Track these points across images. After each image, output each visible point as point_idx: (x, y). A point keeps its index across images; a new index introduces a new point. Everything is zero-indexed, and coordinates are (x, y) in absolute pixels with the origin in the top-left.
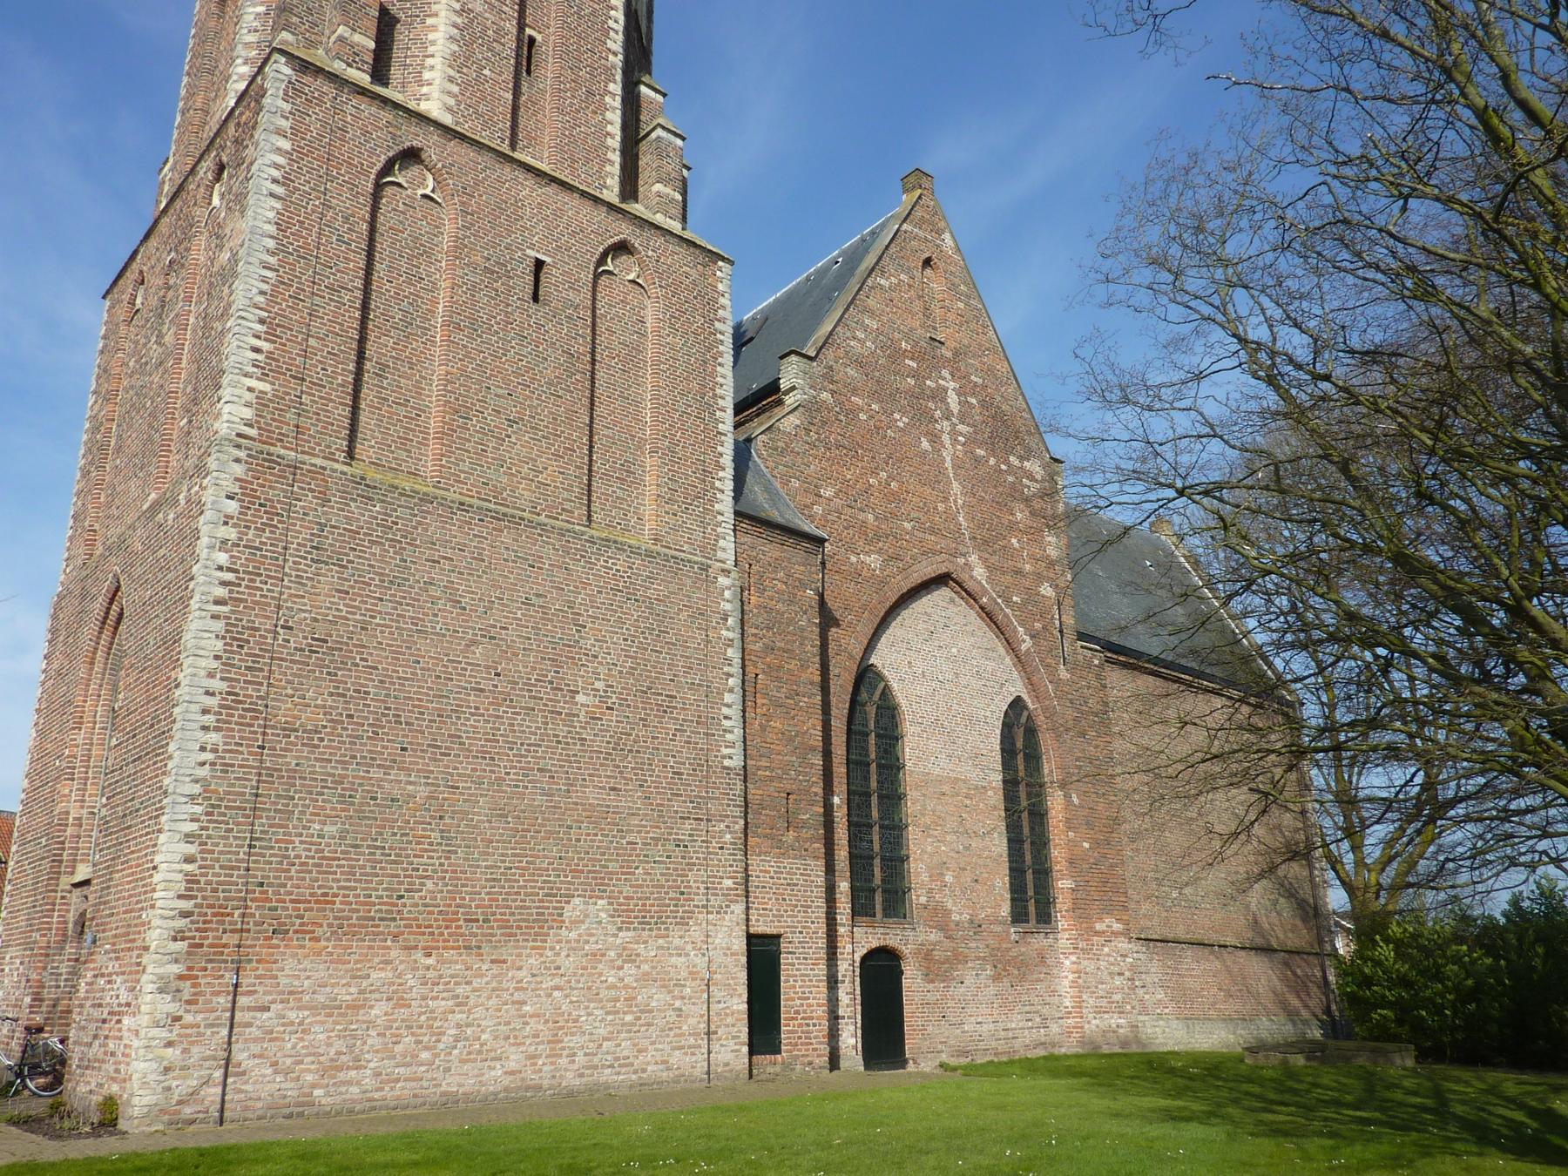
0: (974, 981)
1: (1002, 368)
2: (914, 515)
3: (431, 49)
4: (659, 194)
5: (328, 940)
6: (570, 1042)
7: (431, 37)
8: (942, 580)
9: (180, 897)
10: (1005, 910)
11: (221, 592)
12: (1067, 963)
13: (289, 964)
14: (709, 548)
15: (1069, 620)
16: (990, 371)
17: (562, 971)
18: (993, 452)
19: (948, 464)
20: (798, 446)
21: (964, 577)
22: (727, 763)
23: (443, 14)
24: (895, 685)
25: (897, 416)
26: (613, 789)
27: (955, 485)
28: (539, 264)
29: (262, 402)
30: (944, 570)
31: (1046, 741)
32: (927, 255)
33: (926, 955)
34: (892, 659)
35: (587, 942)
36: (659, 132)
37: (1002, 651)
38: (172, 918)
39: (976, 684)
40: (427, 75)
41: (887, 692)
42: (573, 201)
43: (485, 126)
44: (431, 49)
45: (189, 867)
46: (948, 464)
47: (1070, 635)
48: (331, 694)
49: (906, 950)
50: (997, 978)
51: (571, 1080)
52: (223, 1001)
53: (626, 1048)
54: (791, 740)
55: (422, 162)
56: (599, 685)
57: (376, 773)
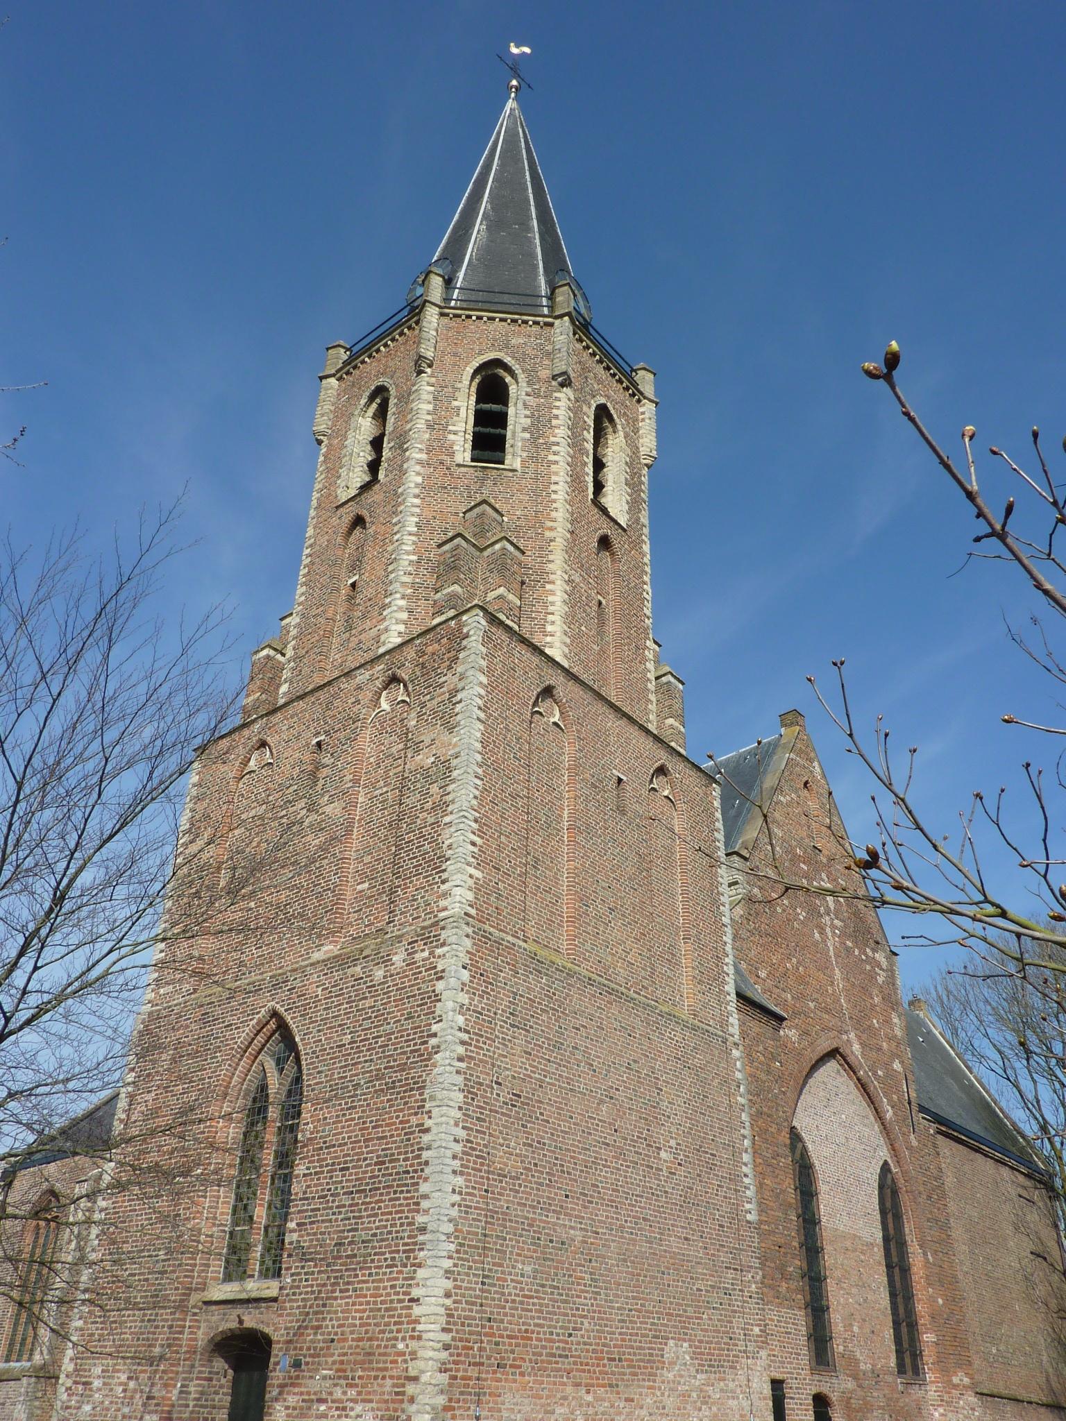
2: (815, 996)
5: (529, 1375)
7: (550, 598)
8: (833, 1053)
9: (443, 1330)
10: (893, 1362)
11: (461, 1050)
12: (936, 1414)
13: (508, 1397)
14: (724, 1024)
17: (666, 1411)
19: (831, 953)
22: (749, 1217)
23: (558, 582)
24: (810, 1146)
25: (799, 910)
26: (686, 1239)
27: (837, 971)
28: (620, 780)
29: (478, 888)
30: (835, 1045)
31: (904, 1198)
32: (805, 779)
35: (679, 1383)
36: (670, 678)
37: (872, 1118)
38: (438, 1350)
39: (860, 1148)
40: (549, 628)
41: (805, 1148)
42: (634, 732)
43: (586, 671)
44: (551, 609)
45: (448, 1302)
46: (831, 953)
47: (915, 1108)
48: (524, 1144)
49: (834, 1397)
54: (777, 1196)
55: (552, 696)
56: (673, 1143)
57: (552, 1218)
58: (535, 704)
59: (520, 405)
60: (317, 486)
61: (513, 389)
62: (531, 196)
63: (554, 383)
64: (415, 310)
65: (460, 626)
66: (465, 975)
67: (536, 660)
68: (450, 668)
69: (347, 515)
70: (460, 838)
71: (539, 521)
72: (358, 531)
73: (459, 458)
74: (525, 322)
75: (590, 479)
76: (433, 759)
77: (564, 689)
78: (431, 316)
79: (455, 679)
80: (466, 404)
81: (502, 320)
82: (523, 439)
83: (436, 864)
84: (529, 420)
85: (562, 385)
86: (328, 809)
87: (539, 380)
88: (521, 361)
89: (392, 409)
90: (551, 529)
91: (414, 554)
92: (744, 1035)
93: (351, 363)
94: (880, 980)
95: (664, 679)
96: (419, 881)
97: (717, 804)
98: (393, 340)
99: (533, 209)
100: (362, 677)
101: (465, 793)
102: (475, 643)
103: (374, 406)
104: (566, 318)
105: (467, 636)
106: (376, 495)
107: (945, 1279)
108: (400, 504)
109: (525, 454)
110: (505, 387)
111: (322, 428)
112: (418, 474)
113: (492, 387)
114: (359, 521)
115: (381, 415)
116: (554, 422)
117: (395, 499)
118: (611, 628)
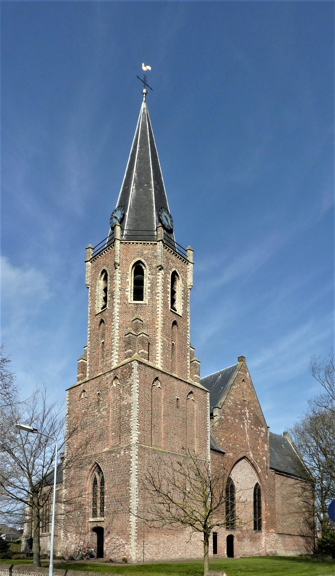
0: (246, 541)
1: (258, 405)
3: (157, 352)
4: (196, 377)
6: (188, 551)
7: (157, 348)
8: (244, 457)
10: (253, 528)
11: (137, 473)
13: (150, 537)
14: (206, 457)
15: (268, 465)
16: (255, 406)
18: (255, 426)
20: (218, 430)
21: (248, 457)
28: (178, 399)
29: (139, 436)
31: (262, 492)
33: (238, 536)
34: (233, 477)
39: (249, 480)
40: (157, 358)
42: (182, 383)
44: (157, 352)
47: (268, 468)
49: (235, 535)
50: (250, 541)
51: (188, 557)
52: (142, 543)
53: (195, 552)
58: (153, 383)
59: (147, 278)
60: (89, 305)
61: (145, 271)
62: (151, 166)
63: (157, 269)
64: (112, 241)
65: (132, 365)
66: (137, 457)
67: (153, 371)
69: (99, 318)
70: (134, 424)
71: (153, 322)
72: (102, 324)
73: (129, 301)
74: (148, 244)
75: (169, 299)
77: (160, 376)
78: (117, 243)
79: (131, 381)
80: (130, 279)
81: (141, 243)
83: (129, 430)
85: (160, 270)
86: (103, 413)
89: (109, 278)
90: (157, 324)
92: (212, 459)
93: (94, 259)
94: (262, 436)
95: (194, 362)
96: (126, 435)
97: (208, 398)
98: (106, 250)
99: (152, 173)
100: (108, 375)
101: (135, 413)
102: (135, 371)
103: (103, 276)
104: (161, 242)
105: (133, 369)
106: (106, 314)
107: (271, 510)
109: (149, 298)
110: (143, 270)
111: (88, 283)
113: (138, 269)
114: (102, 321)
115: (106, 279)
117: (112, 316)
118: (177, 352)
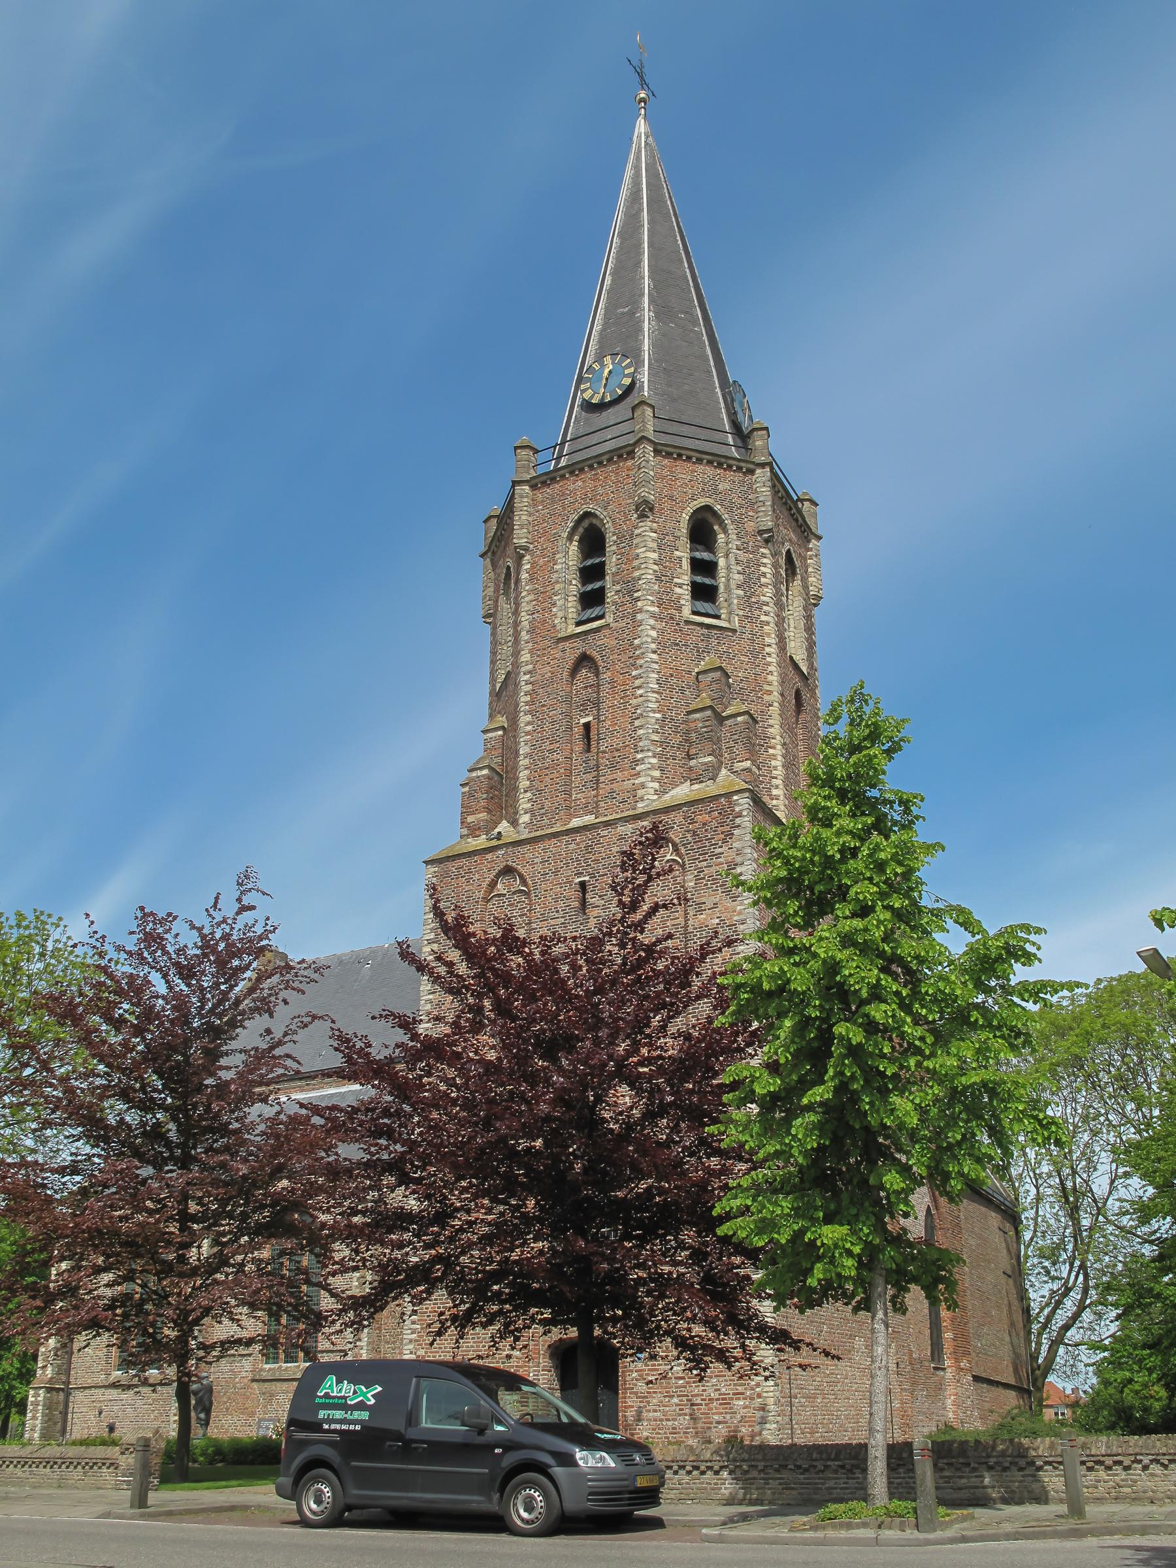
61: (721, 538)
68: (724, 841)
69: (571, 652)
76: (717, 921)
82: (738, 597)
84: (741, 577)
87: (747, 533)
88: (730, 510)
91: (659, 712)
108: (638, 657)
110: (713, 535)
112: (653, 628)
114: (584, 660)
116: (763, 580)
